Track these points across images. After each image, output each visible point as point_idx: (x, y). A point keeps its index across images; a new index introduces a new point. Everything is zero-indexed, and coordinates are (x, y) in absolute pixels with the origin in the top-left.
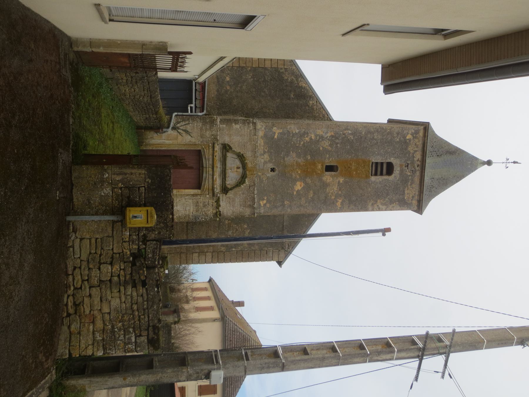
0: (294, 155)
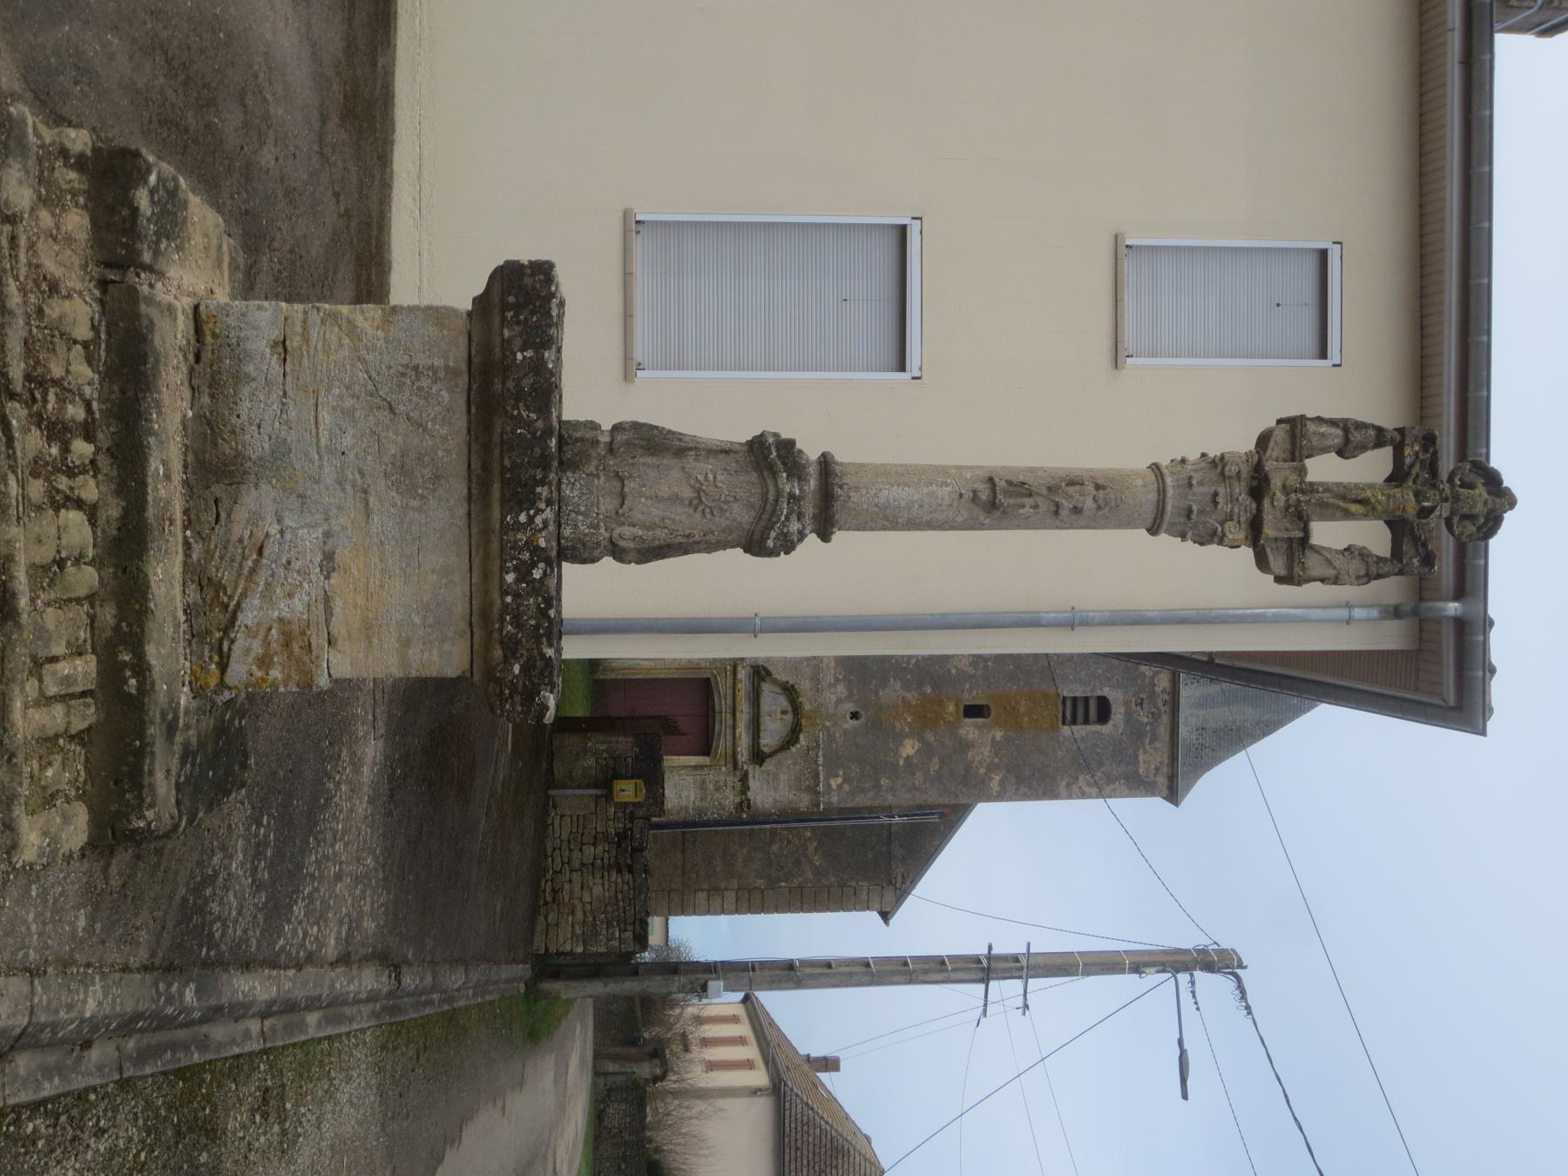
0: (898, 685)
